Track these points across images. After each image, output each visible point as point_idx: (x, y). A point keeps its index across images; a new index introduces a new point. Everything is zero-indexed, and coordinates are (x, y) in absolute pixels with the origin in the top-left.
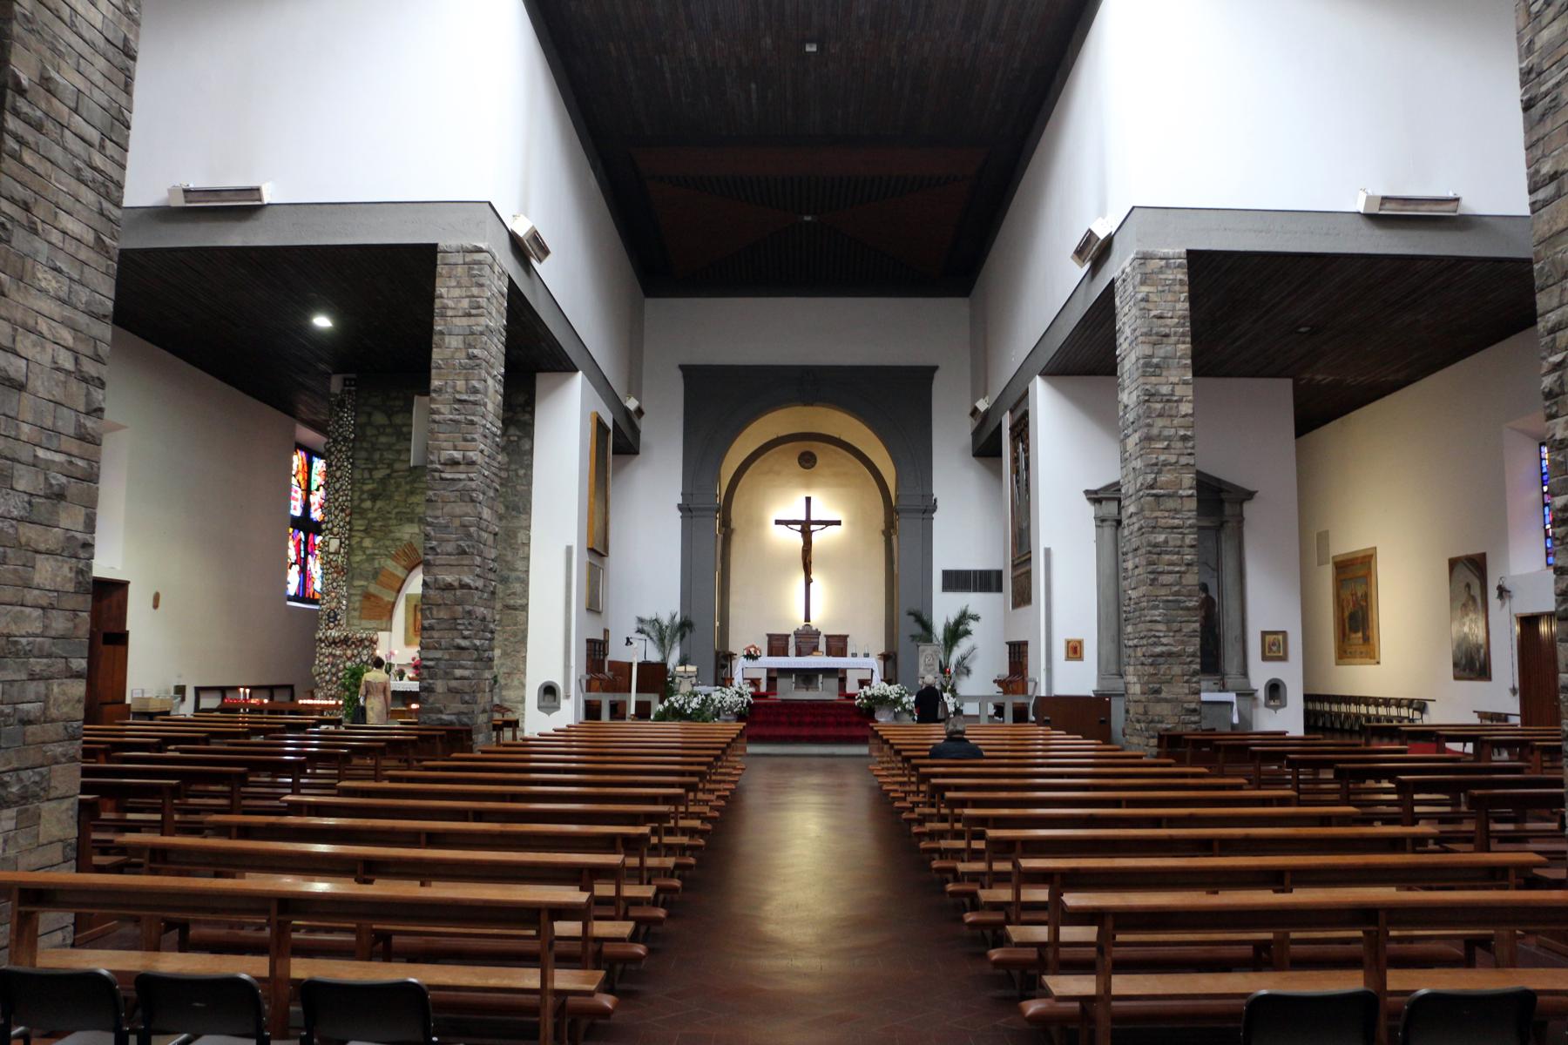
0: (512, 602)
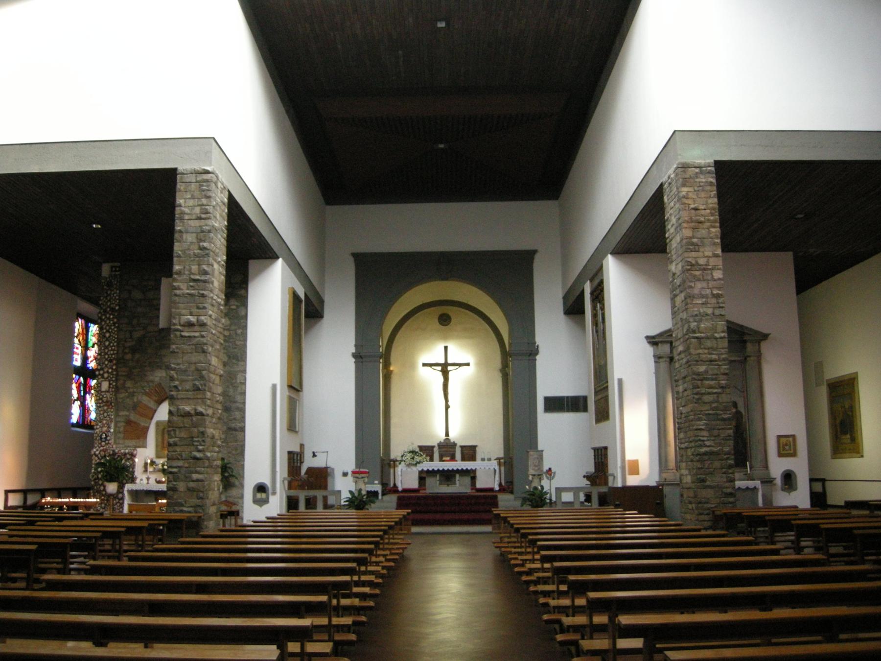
0: (233, 425)
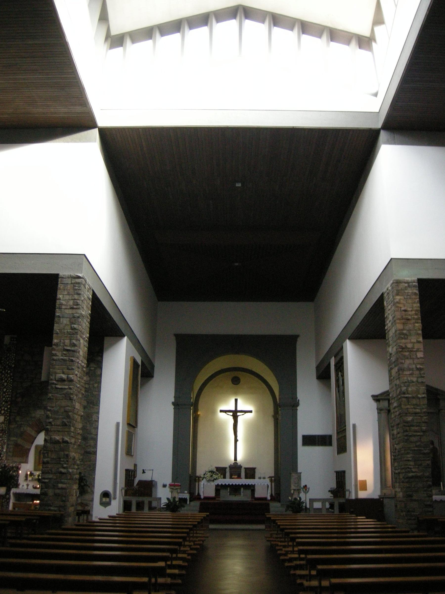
0: (88, 450)
